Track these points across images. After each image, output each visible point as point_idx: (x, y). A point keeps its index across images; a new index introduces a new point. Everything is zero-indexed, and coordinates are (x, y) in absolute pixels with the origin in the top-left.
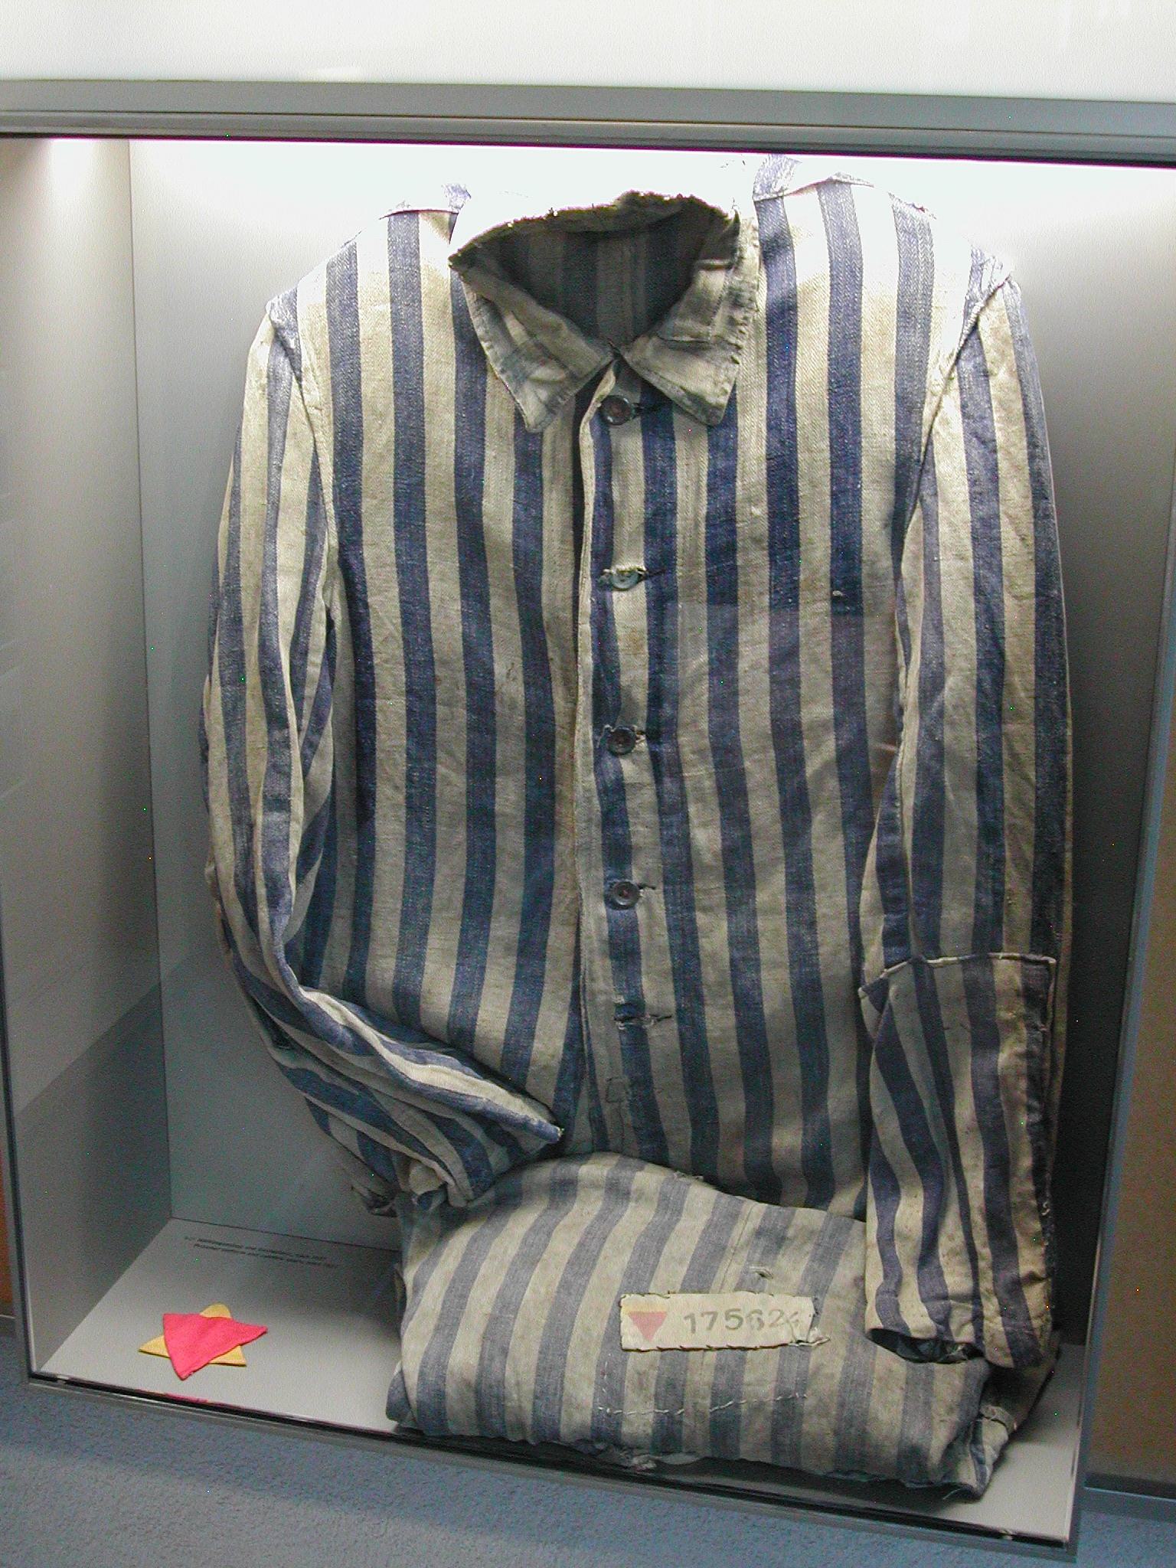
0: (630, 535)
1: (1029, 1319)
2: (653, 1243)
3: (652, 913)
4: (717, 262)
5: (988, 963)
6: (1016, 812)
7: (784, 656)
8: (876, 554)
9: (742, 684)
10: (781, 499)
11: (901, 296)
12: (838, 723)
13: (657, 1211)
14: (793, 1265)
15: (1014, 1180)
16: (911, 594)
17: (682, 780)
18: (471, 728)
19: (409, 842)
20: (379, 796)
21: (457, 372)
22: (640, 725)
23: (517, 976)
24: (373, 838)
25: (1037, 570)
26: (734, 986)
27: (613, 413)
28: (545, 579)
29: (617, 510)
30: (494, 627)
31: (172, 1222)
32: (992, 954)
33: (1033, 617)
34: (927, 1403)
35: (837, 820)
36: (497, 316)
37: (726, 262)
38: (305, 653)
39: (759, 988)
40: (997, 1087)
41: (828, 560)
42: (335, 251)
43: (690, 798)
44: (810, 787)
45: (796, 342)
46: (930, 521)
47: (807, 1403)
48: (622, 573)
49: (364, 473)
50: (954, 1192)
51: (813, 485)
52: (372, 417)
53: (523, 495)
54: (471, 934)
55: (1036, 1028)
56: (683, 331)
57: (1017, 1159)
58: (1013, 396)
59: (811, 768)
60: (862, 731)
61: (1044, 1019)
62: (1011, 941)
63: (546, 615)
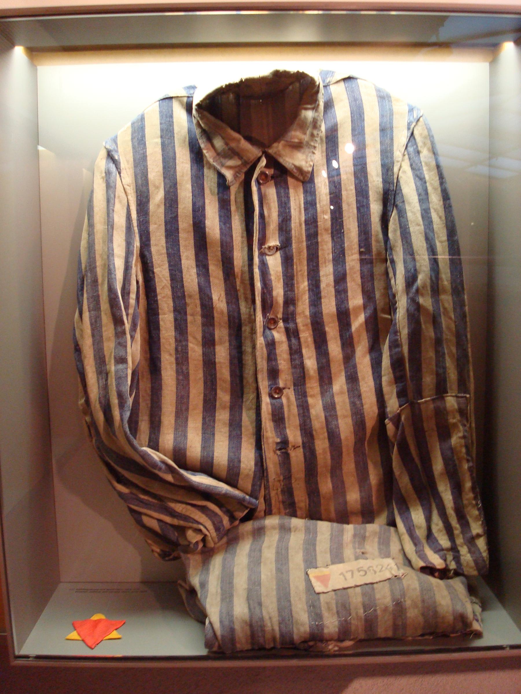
0: (273, 230)
2: (310, 548)
3: (289, 399)
4: (309, 106)
7: (340, 279)
9: (323, 294)
12: (365, 307)
14: (372, 547)
15: (463, 494)
17: (299, 339)
18: (204, 325)
19: (178, 379)
22: (280, 316)
23: (230, 436)
24: (161, 379)
27: (264, 178)
31: (61, 584)
36: (209, 140)
37: (313, 106)
38: (129, 293)
39: (339, 428)
42: (134, 116)
44: (354, 335)
46: (402, 214)
48: (269, 248)
49: (151, 214)
51: (349, 205)
58: (430, 160)
61: (467, 421)
62: (451, 389)
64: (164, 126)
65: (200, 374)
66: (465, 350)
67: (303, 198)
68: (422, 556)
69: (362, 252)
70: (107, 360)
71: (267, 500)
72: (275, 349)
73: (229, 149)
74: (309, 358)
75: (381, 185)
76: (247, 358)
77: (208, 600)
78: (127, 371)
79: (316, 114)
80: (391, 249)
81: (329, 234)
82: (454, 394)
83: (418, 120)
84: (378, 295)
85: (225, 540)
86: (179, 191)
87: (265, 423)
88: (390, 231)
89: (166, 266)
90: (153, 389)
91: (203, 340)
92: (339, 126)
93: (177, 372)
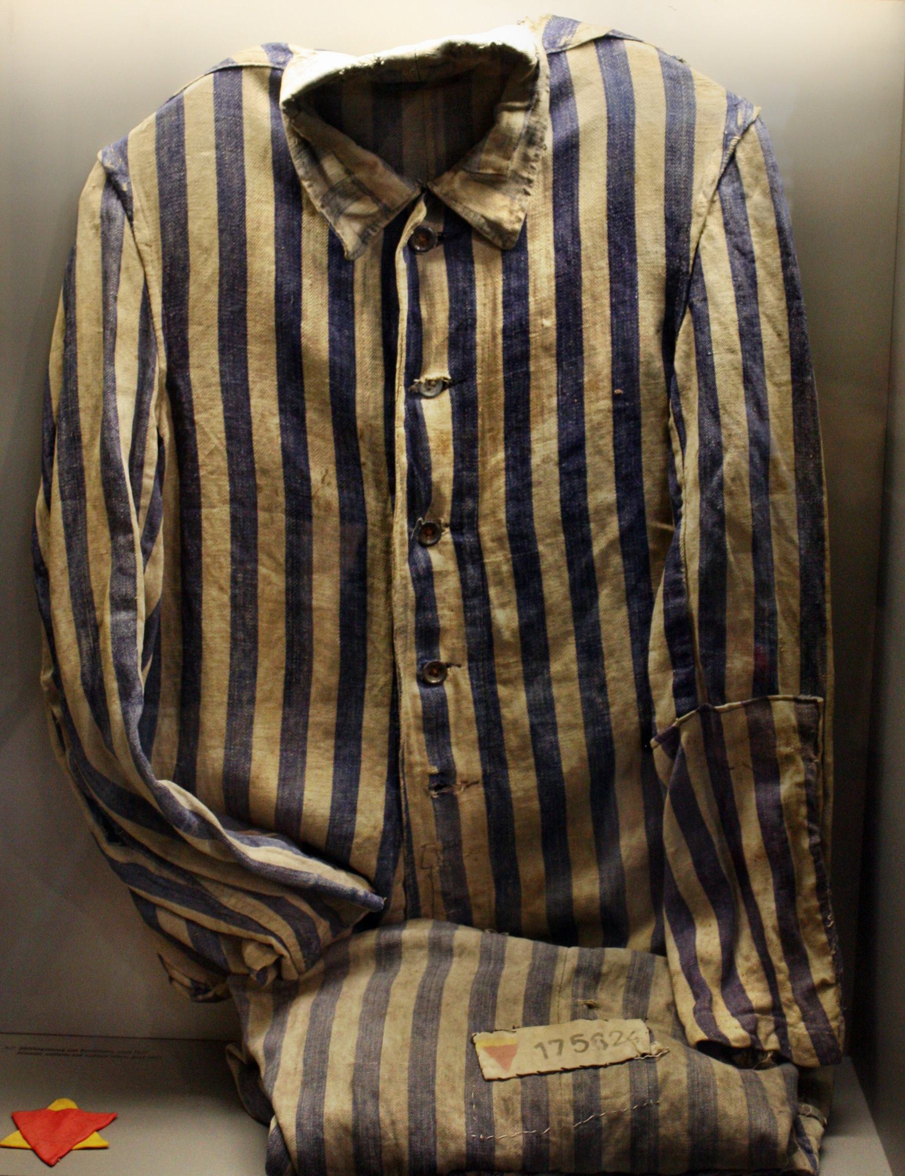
0: (437, 348)
1: (827, 1021)
3: (458, 687)
4: (518, 104)
5: (767, 704)
6: (783, 570)
7: (572, 450)
8: (651, 356)
9: (535, 477)
10: (566, 312)
11: (669, 132)
12: (620, 506)
13: (481, 963)
14: (611, 996)
16: (684, 388)
17: (482, 566)
20: (204, 598)
21: (276, 209)
22: (445, 519)
23: (336, 758)
25: (792, 360)
26: (535, 747)
28: (359, 391)
29: (425, 326)
30: (310, 438)
32: (770, 697)
33: (790, 401)
34: (764, 1098)
35: (621, 593)
36: (315, 159)
37: (526, 104)
38: (141, 466)
40: (781, 816)
41: (609, 363)
43: (491, 580)
44: (597, 564)
45: (578, 175)
46: (701, 324)
47: (660, 1109)
48: (429, 382)
49: (191, 303)
50: (744, 919)
52: (198, 252)
53: (336, 318)
54: (292, 721)
55: (811, 760)
56: (487, 165)
57: (801, 879)
58: (766, 214)
59: (598, 546)
60: (641, 512)
61: (816, 754)
62: (785, 685)
63: (359, 423)
64: (224, 126)
65: (280, 630)
66: (819, 608)
67: (501, 283)
68: (704, 1015)
69: (619, 395)
70: (96, 599)
71: (411, 887)
72: (432, 586)
73: (353, 182)
74: (503, 606)
75: (663, 262)
76: (375, 601)
77: (277, 1083)
78: (136, 624)
79: (534, 119)
80: (678, 394)
81: (551, 356)
82: (791, 696)
83: (746, 130)
84: (648, 484)
85: (320, 966)
86: (249, 259)
87: (408, 735)
88: (677, 356)
89: (219, 409)
90: (185, 653)
91: (287, 561)
92: (581, 137)
93: (234, 624)
